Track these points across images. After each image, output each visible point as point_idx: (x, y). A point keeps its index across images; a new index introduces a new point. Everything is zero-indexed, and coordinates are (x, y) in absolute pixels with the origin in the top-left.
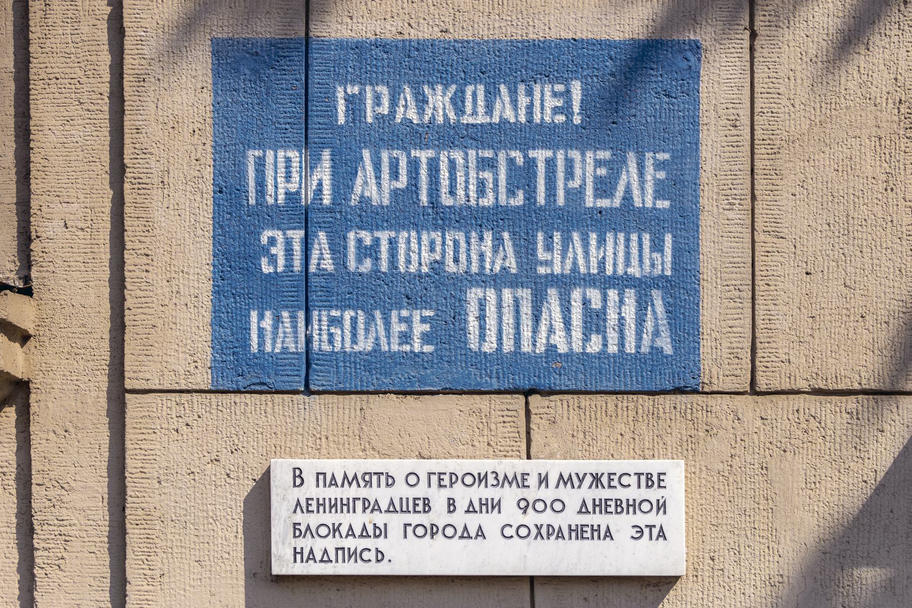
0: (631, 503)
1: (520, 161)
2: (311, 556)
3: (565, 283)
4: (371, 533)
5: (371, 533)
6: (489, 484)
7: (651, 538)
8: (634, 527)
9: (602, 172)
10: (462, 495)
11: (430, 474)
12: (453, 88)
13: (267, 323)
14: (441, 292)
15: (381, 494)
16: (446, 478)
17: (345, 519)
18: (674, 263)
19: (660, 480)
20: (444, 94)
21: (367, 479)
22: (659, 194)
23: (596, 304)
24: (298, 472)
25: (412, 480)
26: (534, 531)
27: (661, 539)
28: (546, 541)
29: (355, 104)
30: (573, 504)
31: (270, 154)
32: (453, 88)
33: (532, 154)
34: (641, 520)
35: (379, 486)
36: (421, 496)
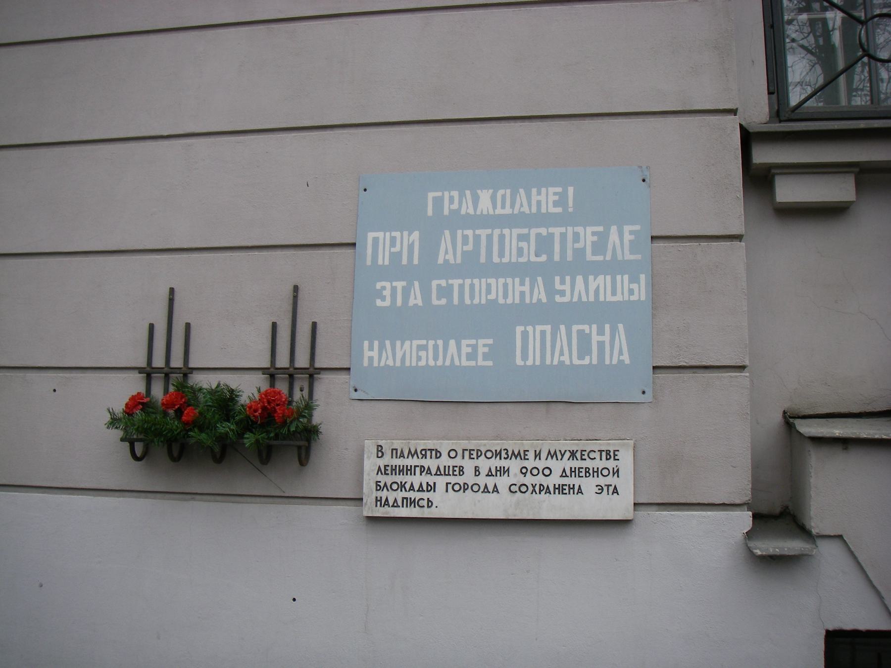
4: (425, 488)
5: (425, 488)
10: (484, 464)
11: (464, 450)
15: (431, 463)
16: (475, 453)
17: (408, 479)
19: (615, 455)
25: (453, 454)
26: (531, 489)
34: (602, 481)
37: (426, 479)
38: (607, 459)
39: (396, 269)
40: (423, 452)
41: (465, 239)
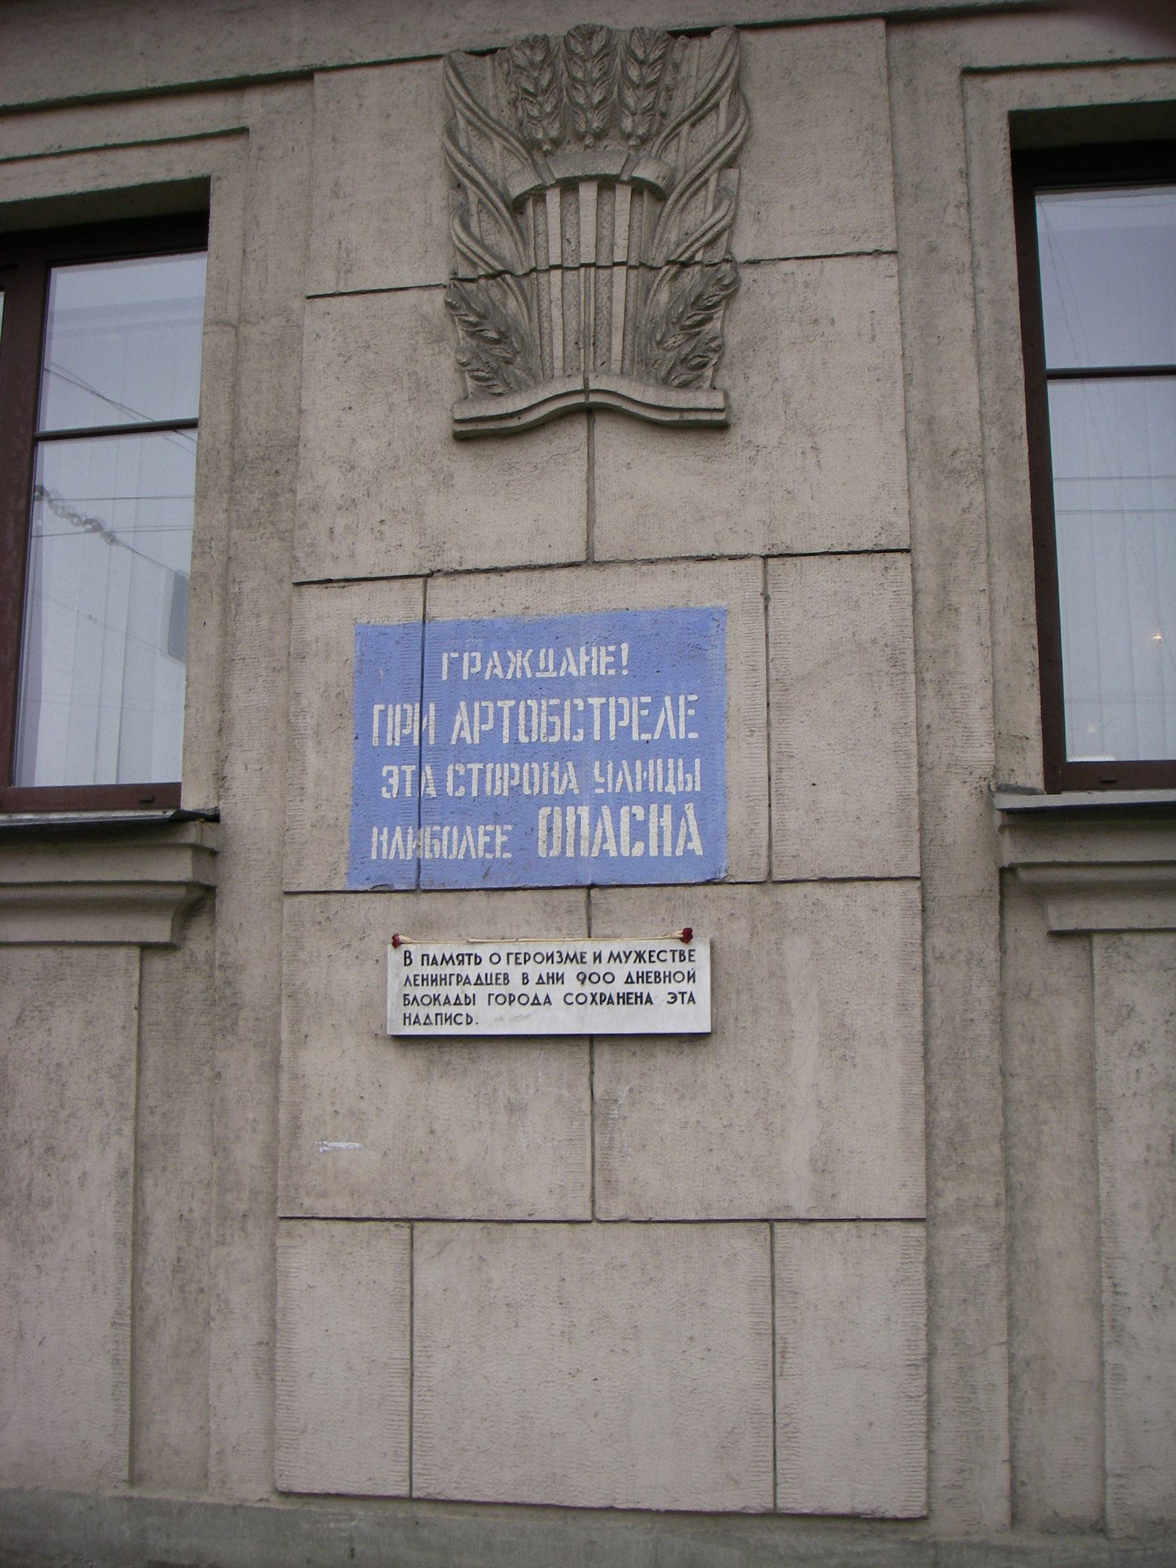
10: (534, 970)
14: (517, 810)
17: (442, 991)
20: (523, 657)
23: (640, 817)
26: (590, 999)
29: (455, 665)
30: (621, 977)
34: (674, 987)
41: (484, 711)
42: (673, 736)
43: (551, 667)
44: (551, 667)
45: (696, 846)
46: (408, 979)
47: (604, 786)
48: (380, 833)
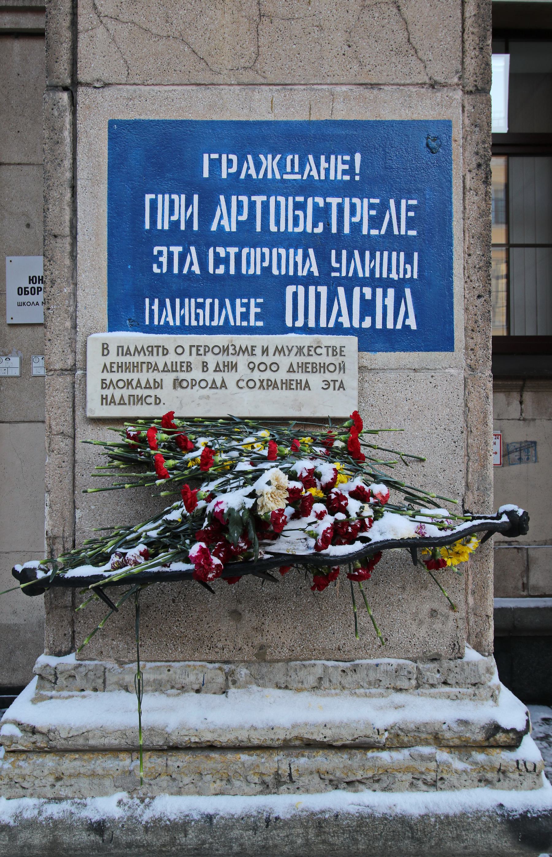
0: (322, 365)
1: (322, 204)
2: (113, 401)
3: (349, 283)
4: (152, 385)
5: (152, 385)
6: (230, 353)
7: (334, 389)
8: (324, 381)
9: (373, 213)
10: (211, 360)
11: (191, 347)
12: (279, 156)
13: (156, 307)
15: (161, 361)
16: (202, 349)
17: (134, 376)
18: (419, 271)
19: (341, 351)
20: (273, 159)
21: (151, 350)
22: (409, 227)
23: (368, 297)
24: (105, 346)
25: (180, 350)
26: (258, 384)
27: (341, 389)
28: (266, 391)
29: (215, 165)
30: (284, 367)
31: (160, 197)
32: (279, 156)
33: (329, 200)
34: (328, 376)
35: (158, 355)
36: (186, 361)
37: (152, 376)
38: (333, 355)
39: (174, 235)
40: (150, 349)
41: (240, 205)
42: (396, 232)
43: (296, 169)
44: (296, 169)
45: (412, 322)
46: (105, 365)
47: (339, 270)
48: (151, 304)
